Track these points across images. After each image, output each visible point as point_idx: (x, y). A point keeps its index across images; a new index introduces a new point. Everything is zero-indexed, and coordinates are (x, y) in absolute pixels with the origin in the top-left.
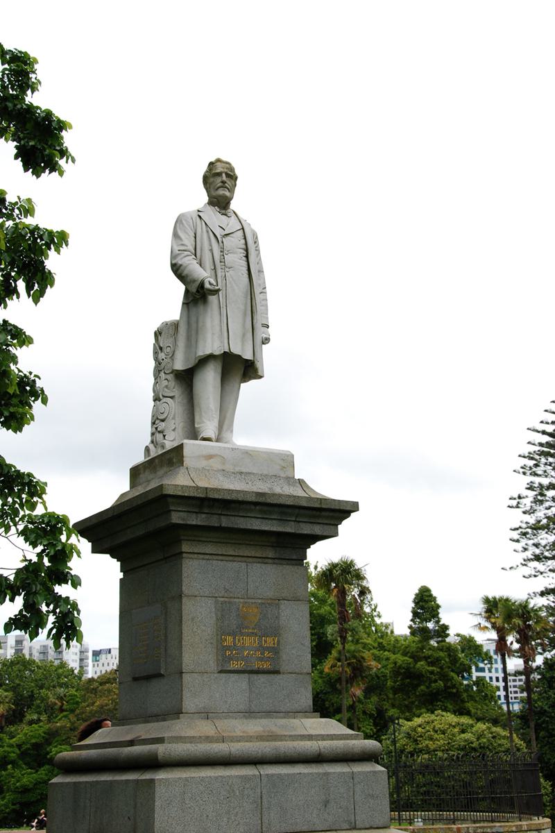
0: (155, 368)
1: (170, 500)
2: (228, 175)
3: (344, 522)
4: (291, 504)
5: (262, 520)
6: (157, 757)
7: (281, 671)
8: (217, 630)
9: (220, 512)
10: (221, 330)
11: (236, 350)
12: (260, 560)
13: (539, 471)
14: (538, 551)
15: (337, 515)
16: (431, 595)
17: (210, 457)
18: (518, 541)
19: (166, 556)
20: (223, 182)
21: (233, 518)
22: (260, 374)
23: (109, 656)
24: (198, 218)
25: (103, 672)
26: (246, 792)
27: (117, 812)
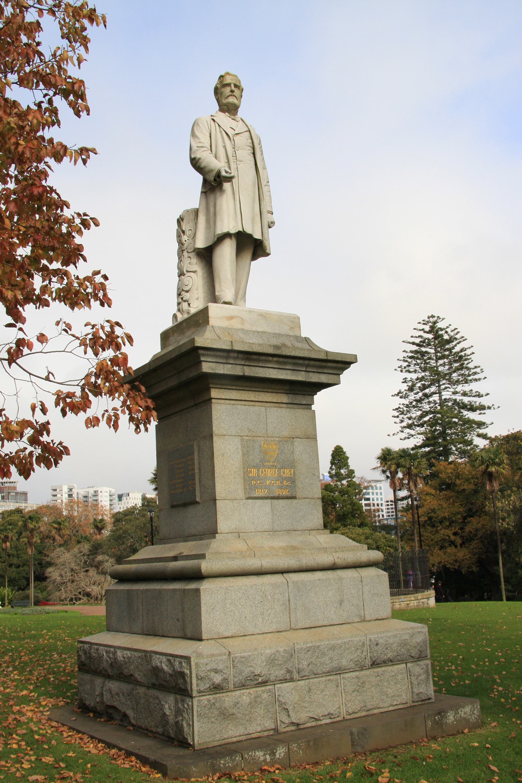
0: (179, 249)
1: (201, 352)
2: (236, 86)
3: (345, 372)
4: (302, 356)
5: (277, 370)
6: (201, 570)
7: (297, 496)
8: (244, 464)
9: (243, 363)
10: (235, 209)
11: (248, 230)
12: (276, 405)
13: (412, 369)
14: (410, 422)
15: (340, 365)
16: (342, 451)
17: (231, 318)
18: (398, 417)
19: (196, 402)
20: (232, 91)
21: (254, 368)
22: (268, 251)
23: (128, 497)
24: (212, 121)
25: (125, 508)
26: (276, 596)
27: (167, 614)
